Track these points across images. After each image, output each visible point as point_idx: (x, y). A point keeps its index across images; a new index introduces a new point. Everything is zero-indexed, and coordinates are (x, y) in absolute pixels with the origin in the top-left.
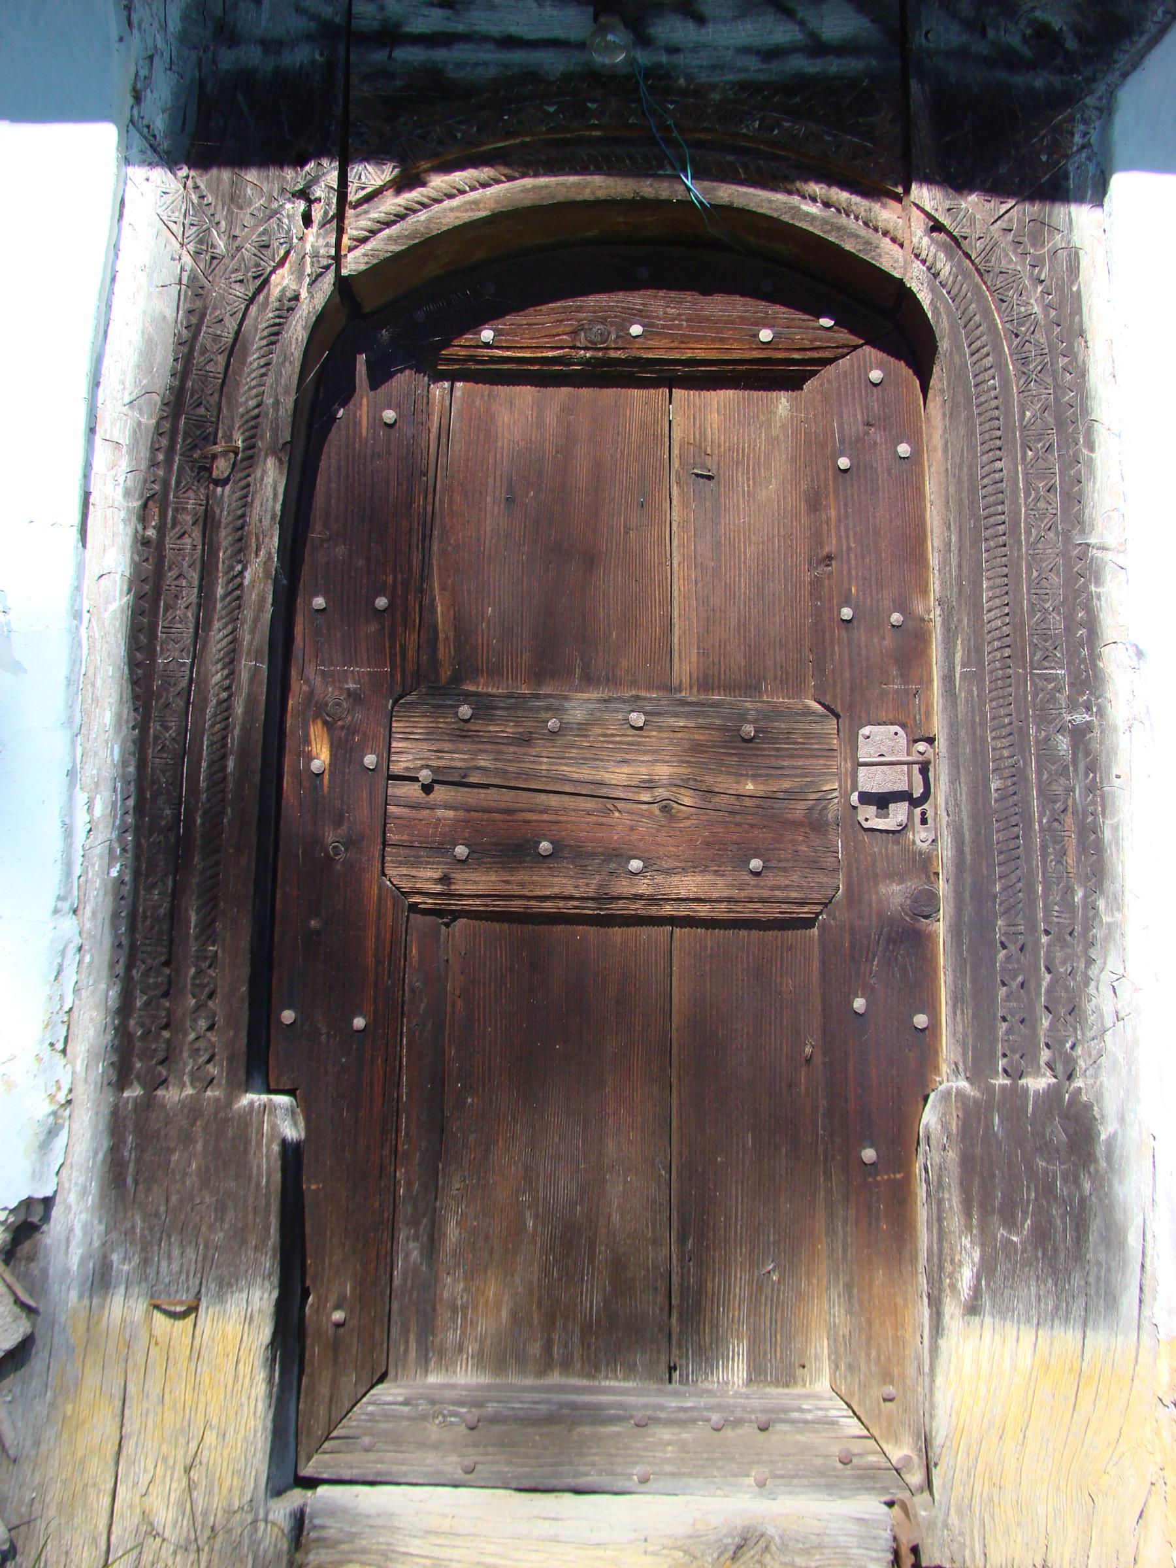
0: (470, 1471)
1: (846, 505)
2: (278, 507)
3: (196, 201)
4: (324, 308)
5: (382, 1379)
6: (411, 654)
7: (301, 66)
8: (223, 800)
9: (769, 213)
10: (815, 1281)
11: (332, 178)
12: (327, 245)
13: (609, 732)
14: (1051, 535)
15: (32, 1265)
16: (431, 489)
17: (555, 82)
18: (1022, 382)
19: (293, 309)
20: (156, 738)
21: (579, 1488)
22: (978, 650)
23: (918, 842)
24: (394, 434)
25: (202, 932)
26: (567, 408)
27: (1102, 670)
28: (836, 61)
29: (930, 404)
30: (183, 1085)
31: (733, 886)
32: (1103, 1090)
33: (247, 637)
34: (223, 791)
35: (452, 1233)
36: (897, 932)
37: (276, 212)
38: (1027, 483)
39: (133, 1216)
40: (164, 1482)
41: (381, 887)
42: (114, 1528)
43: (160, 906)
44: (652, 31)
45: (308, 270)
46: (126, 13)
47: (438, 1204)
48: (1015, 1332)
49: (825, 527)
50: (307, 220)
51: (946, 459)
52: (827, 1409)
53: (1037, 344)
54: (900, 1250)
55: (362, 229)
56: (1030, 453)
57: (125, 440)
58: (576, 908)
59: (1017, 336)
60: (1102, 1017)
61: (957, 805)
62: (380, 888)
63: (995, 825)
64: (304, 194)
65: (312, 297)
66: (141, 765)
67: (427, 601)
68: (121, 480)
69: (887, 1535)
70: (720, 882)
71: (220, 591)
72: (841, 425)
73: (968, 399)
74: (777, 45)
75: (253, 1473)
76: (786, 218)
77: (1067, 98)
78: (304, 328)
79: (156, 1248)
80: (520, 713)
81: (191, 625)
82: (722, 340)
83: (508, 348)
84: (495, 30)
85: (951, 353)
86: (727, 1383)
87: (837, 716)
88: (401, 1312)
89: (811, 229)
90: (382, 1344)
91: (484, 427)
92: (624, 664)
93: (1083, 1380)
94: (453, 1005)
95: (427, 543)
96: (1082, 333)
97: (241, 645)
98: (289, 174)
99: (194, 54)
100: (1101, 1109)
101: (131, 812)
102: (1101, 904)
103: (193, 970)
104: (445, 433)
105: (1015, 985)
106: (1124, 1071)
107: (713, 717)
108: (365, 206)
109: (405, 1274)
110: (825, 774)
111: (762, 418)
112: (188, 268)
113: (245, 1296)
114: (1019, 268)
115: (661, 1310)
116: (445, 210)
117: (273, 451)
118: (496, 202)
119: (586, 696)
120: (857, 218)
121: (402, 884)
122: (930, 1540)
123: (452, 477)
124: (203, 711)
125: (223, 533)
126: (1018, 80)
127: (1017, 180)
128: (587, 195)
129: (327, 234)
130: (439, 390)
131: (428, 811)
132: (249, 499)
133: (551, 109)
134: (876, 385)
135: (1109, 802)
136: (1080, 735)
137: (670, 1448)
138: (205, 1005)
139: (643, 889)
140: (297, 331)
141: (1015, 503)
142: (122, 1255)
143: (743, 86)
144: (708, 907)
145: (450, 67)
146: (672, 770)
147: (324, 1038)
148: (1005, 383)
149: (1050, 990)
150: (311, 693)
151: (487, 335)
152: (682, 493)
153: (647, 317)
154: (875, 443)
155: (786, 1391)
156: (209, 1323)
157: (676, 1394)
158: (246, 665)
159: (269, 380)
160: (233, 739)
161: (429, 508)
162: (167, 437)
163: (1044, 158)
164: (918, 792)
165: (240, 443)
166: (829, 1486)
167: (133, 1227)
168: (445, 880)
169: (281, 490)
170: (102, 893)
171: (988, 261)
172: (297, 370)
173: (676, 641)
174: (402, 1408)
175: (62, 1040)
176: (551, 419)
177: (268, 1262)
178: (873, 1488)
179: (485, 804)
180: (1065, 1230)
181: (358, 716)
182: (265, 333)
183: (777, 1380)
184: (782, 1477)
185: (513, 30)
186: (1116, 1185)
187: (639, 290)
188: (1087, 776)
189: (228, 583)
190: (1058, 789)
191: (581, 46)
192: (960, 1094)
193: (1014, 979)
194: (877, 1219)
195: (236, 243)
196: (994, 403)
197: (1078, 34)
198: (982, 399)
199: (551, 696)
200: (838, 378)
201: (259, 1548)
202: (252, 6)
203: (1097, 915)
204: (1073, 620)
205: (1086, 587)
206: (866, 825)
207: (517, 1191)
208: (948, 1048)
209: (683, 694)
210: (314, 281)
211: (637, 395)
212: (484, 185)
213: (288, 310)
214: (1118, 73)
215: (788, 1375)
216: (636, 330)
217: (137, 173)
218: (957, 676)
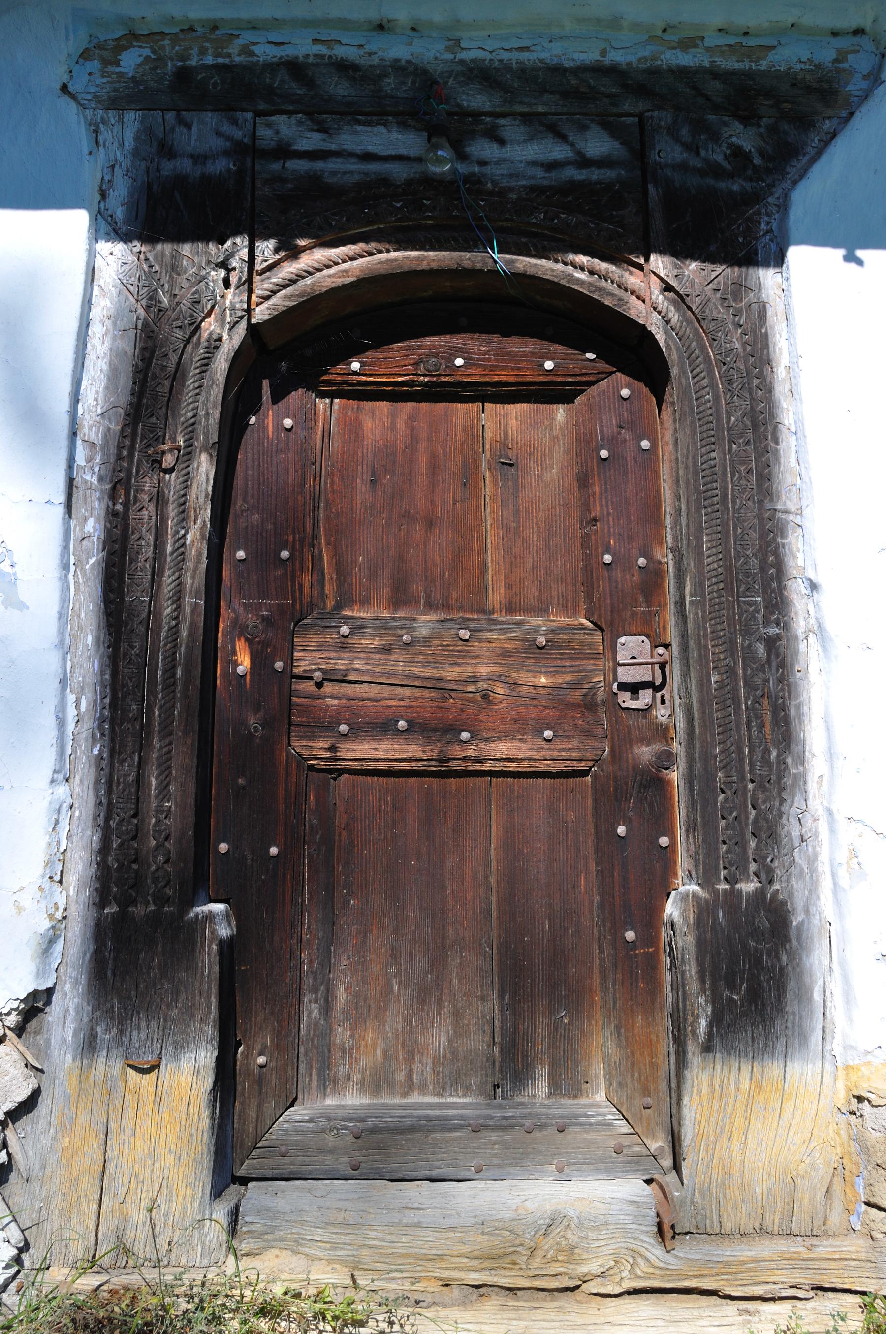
0: (355, 1168)
1: (606, 484)
2: (210, 489)
3: (146, 270)
4: (240, 347)
5: (292, 1105)
6: (307, 590)
7: (221, 172)
8: (174, 698)
9: (551, 278)
10: (594, 1023)
11: (244, 253)
12: (241, 301)
13: (445, 643)
14: (750, 503)
15: (38, 1037)
16: (318, 474)
17: (400, 185)
18: (728, 396)
19: (218, 347)
20: (125, 654)
21: (434, 1177)
22: (702, 585)
23: (659, 716)
24: (292, 435)
25: (160, 793)
26: (412, 418)
27: (787, 597)
28: (596, 172)
29: (664, 413)
30: (147, 904)
31: (532, 749)
32: (794, 891)
33: (189, 581)
34: (174, 691)
35: (342, 996)
36: (646, 780)
37: (204, 278)
38: (733, 467)
39: (112, 999)
40: (136, 1193)
41: (288, 754)
42: (100, 1227)
43: (129, 775)
44: (468, 149)
45: (228, 320)
46: (94, 135)
47: (331, 976)
48: (737, 1064)
49: (592, 499)
50: (227, 283)
51: (677, 451)
52: (605, 1115)
53: (738, 370)
54: (653, 1002)
55: (266, 290)
56: (734, 446)
57: (98, 441)
58: (424, 766)
59: (724, 364)
60: (792, 840)
61: (687, 692)
62: (287, 756)
63: (715, 707)
64: (224, 265)
65: (231, 338)
66: (115, 674)
67: (316, 553)
68: (97, 469)
69: (653, 1213)
70: (524, 746)
71: (169, 549)
72: (601, 427)
73: (692, 409)
74: (555, 160)
75: (201, 1184)
76: (563, 282)
77: (755, 198)
78: (226, 361)
79: (129, 1022)
80: (383, 631)
81: (149, 573)
82: (519, 369)
83: (370, 375)
84: (358, 149)
85: (679, 378)
86: (534, 1096)
87: (602, 630)
88: (306, 1054)
89: (581, 290)
90: (293, 1079)
91: (354, 430)
92: (454, 594)
93: (785, 1097)
94: (340, 835)
95: (316, 512)
96: (769, 362)
97: (185, 587)
98: (212, 247)
99: (143, 164)
100: (792, 904)
101: (107, 707)
102: (789, 760)
103: (154, 820)
104: (327, 434)
105: (731, 818)
106: (807, 878)
107: (516, 632)
108: (268, 274)
109: (308, 1026)
110: (594, 670)
111: (547, 423)
112: (142, 317)
113: (194, 1056)
114: (725, 316)
115: (488, 1046)
116: (324, 277)
117: (205, 448)
118: (361, 271)
119: (428, 618)
120: (612, 282)
121: (303, 752)
122: (681, 1215)
123: (333, 465)
124: (159, 634)
125: (171, 507)
126: (722, 185)
127: (722, 255)
128: (424, 266)
129: (241, 293)
130: (322, 404)
131: (320, 701)
132: (189, 483)
133: (398, 205)
134: (625, 399)
135: (793, 689)
136: (772, 643)
137: (496, 1147)
138: (163, 845)
139: (471, 752)
140: (221, 364)
141: (724, 480)
142: (105, 1027)
143: (532, 189)
144: (515, 764)
145: (326, 174)
146: (489, 669)
147: (249, 861)
148: (717, 398)
149: (756, 821)
150: (236, 619)
151: (356, 366)
152: (493, 476)
153: (467, 353)
154: (625, 440)
155: (576, 1102)
156: (168, 1075)
157: (500, 1106)
158: (188, 601)
159: (202, 398)
160: (180, 654)
161: (317, 488)
162: (129, 438)
163: (741, 240)
164: (658, 682)
165: (181, 444)
166: (608, 1170)
167: (112, 1007)
168: (333, 748)
169: (212, 477)
170: (87, 766)
171: (704, 312)
172: (222, 391)
173: (490, 579)
174: (308, 1125)
175: (59, 873)
176: (401, 425)
177: (210, 1030)
178: (638, 1170)
179: (360, 695)
180: (770, 990)
181: (270, 634)
182: (198, 364)
183: (569, 1094)
184: (575, 1164)
185: (371, 148)
186: (804, 958)
187: (459, 333)
188: (777, 671)
189: (175, 543)
190: (758, 681)
191: (419, 160)
192: (695, 895)
193: (731, 814)
194: (637, 981)
195: (176, 300)
196: (709, 412)
197: (761, 153)
198: (701, 409)
199: (404, 618)
200: (599, 395)
201: (205, 1240)
202: (185, 131)
203: (786, 768)
204: (766, 562)
205: (774, 539)
206: (624, 706)
207: (387, 966)
208: (683, 862)
209: (495, 616)
210: (233, 327)
211: (460, 408)
212: (352, 259)
213: (214, 348)
214: (789, 181)
215: (576, 1092)
216: (459, 362)
217: (104, 247)
218: (687, 603)
